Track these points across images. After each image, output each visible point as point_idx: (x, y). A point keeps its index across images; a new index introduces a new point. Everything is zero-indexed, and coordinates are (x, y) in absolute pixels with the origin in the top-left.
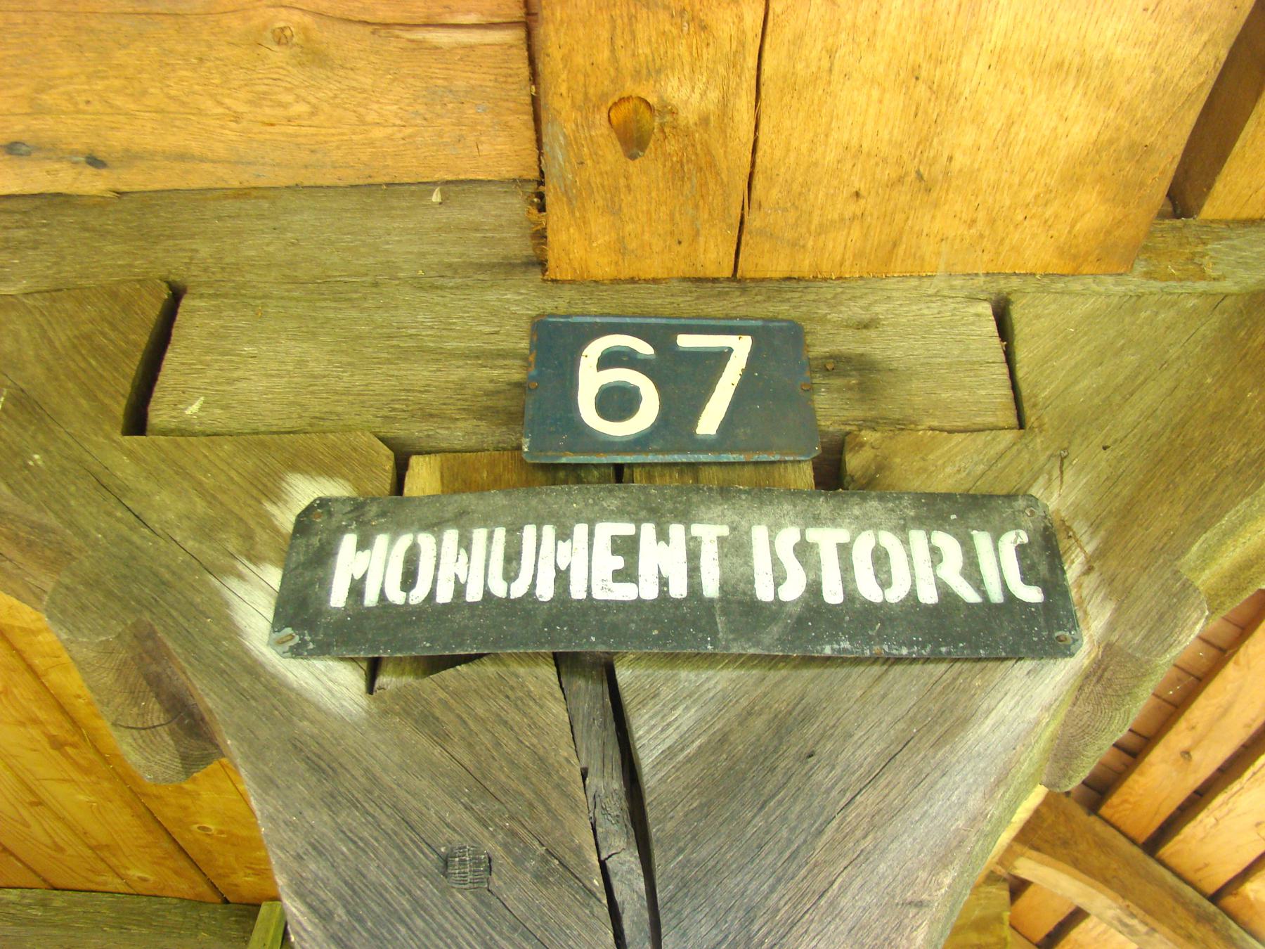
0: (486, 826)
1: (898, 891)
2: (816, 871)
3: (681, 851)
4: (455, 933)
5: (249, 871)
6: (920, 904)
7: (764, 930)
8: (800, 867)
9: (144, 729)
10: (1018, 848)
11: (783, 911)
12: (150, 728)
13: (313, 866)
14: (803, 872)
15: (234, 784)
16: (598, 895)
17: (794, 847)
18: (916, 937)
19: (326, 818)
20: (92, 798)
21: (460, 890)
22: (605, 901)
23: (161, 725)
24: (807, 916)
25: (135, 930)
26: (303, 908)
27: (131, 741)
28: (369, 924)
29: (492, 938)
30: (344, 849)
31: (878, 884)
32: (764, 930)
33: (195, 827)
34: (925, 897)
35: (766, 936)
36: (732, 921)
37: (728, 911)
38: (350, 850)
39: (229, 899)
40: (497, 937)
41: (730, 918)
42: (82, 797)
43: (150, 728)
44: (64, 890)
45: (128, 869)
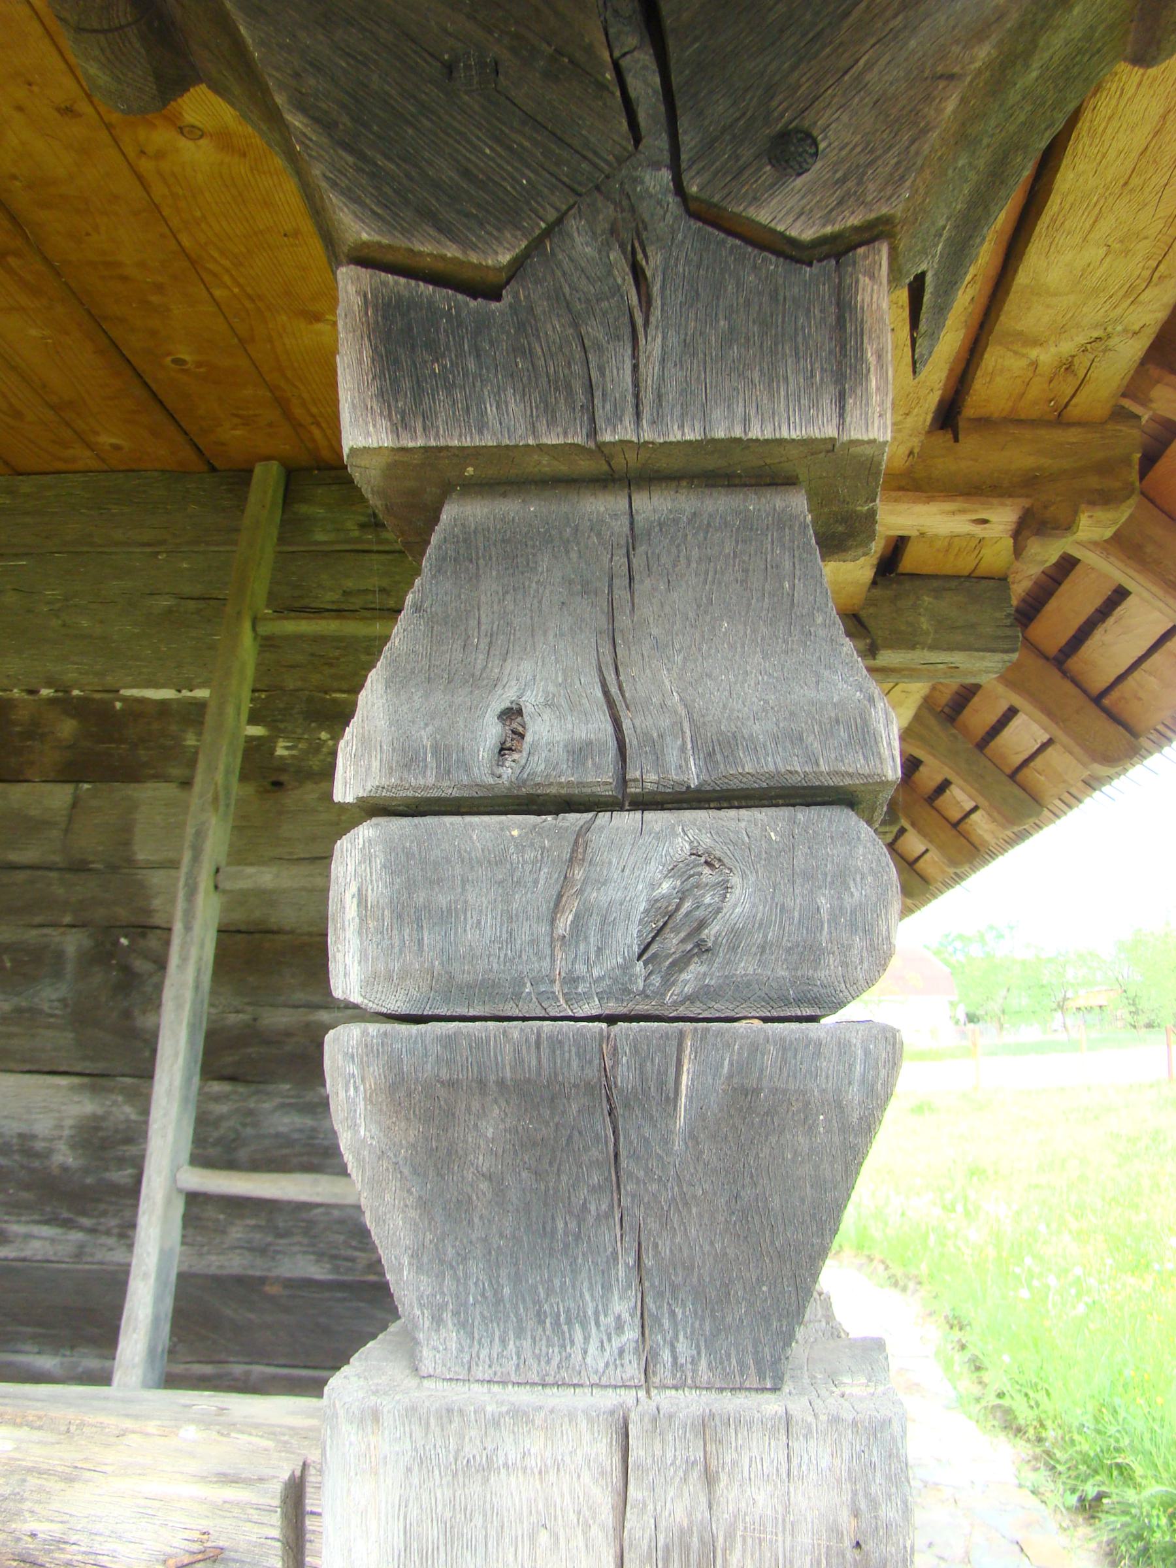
0: (490, 32)
1: (929, 64)
2: (840, 50)
3: (696, 39)
4: (463, 129)
5: (236, 420)
6: (951, 77)
7: (785, 104)
8: (823, 47)
9: (110, 30)
10: (1154, 371)
11: (803, 88)
12: (117, 29)
13: (312, 82)
14: (828, 50)
15: (208, 289)
16: (611, 88)
17: (818, 29)
18: (945, 108)
19: (321, 37)
20: (47, 332)
21: (466, 93)
22: (618, 94)
23: (129, 25)
24: (829, 91)
25: (115, 510)
26: (305, 120)
27: (97, 52)
28: (375, 128)
29: (501, 130)
30: (344, 64)
31: (906, 59)
32: (785, 104)
33: (169, 359)
34: (956, 70)
35: (786, 110)
36: (751, 99)
37: (746, 90)
38: (348, 64)
39: (217, 464)
40: (507, 131)
41: (748, 97)
42: (34, 332)
43: (117, 29)
44: (29, 474)
45: (97, 433)
